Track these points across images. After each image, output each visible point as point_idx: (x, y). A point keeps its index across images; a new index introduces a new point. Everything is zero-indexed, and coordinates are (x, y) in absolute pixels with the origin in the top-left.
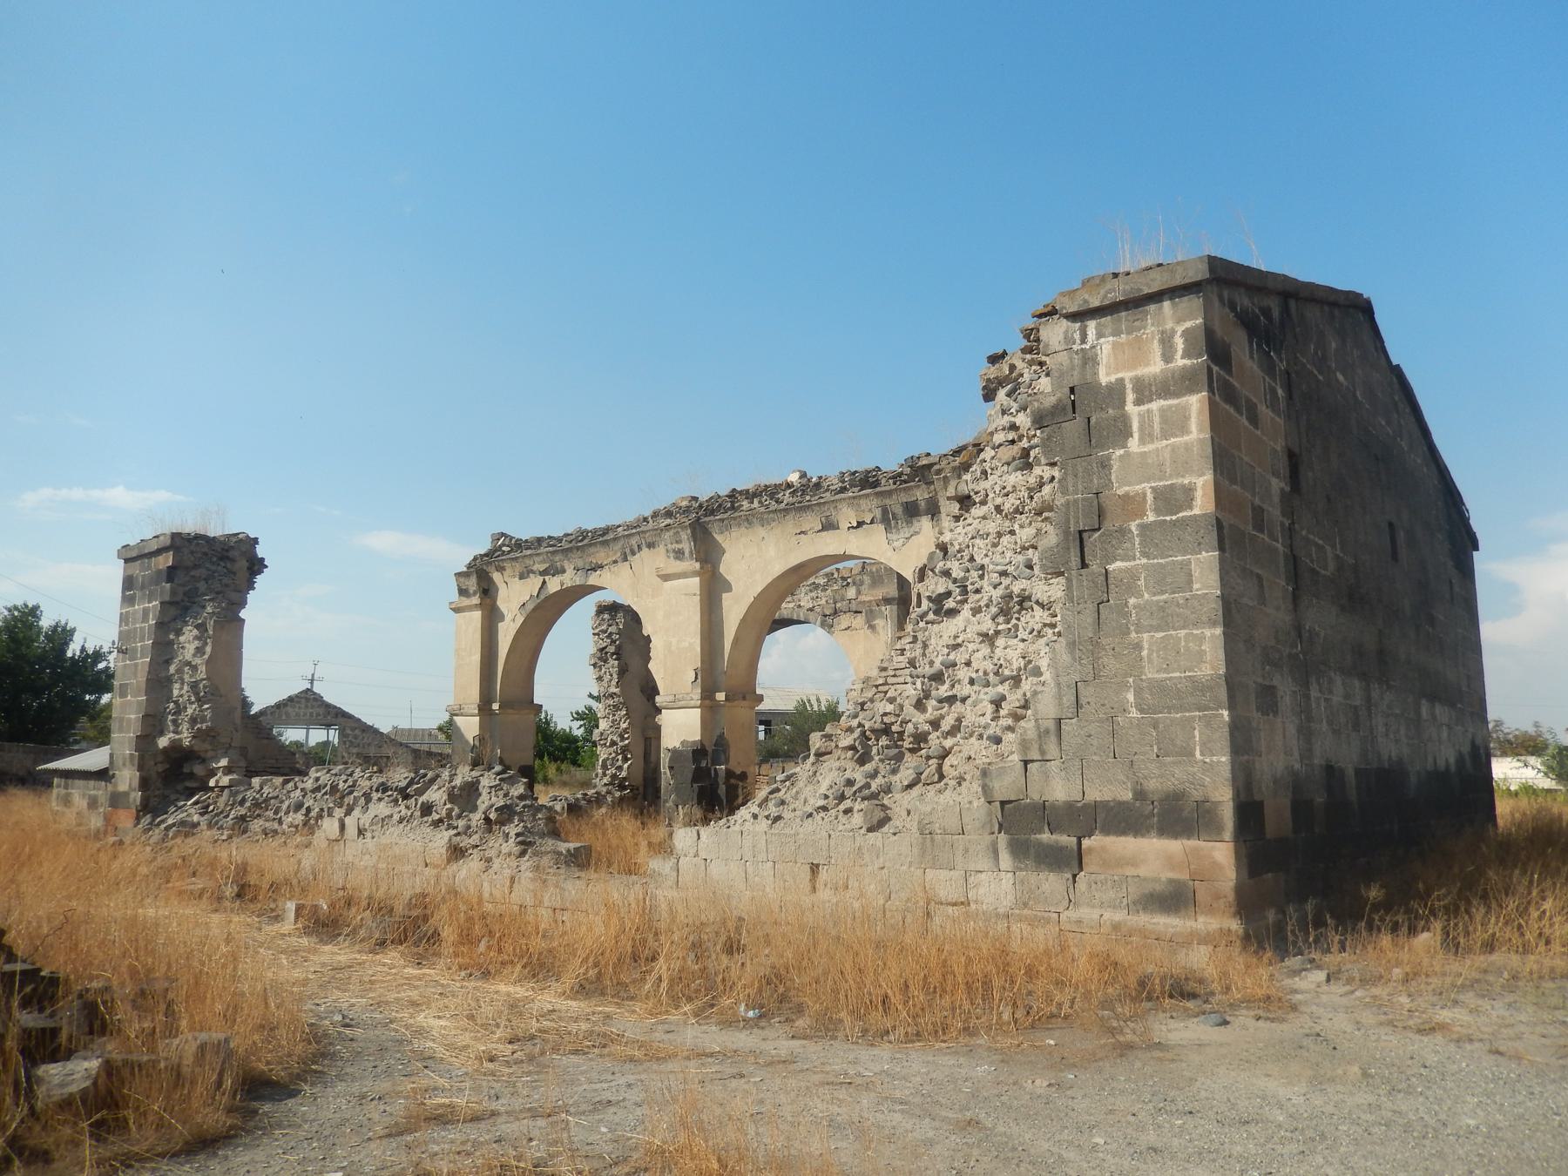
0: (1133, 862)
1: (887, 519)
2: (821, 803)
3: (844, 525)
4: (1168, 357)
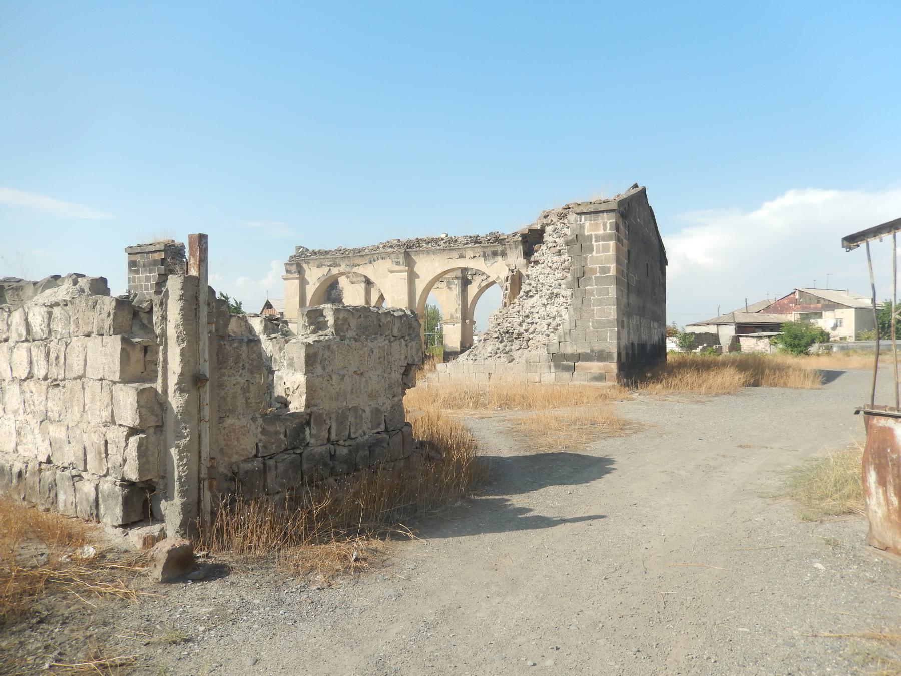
0: (590, 368)
1: (485, 256)
2: (490, 354)
3: (468, 257)
4: (605, 230)
